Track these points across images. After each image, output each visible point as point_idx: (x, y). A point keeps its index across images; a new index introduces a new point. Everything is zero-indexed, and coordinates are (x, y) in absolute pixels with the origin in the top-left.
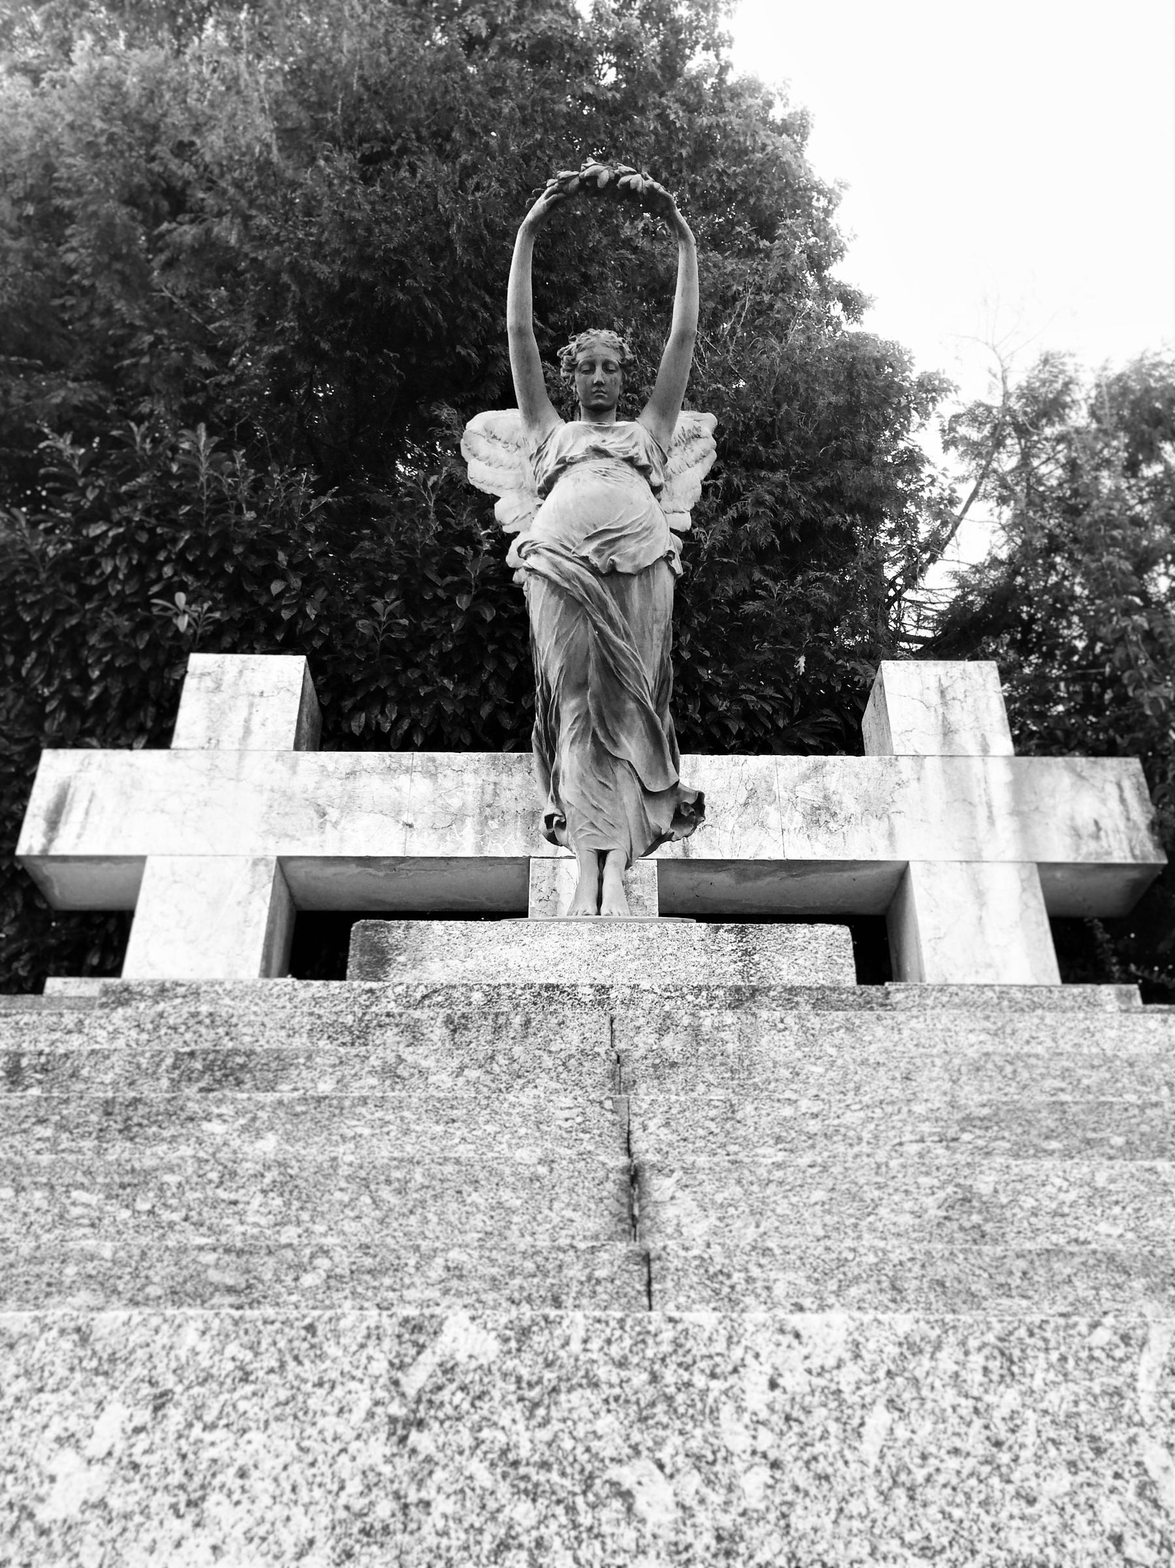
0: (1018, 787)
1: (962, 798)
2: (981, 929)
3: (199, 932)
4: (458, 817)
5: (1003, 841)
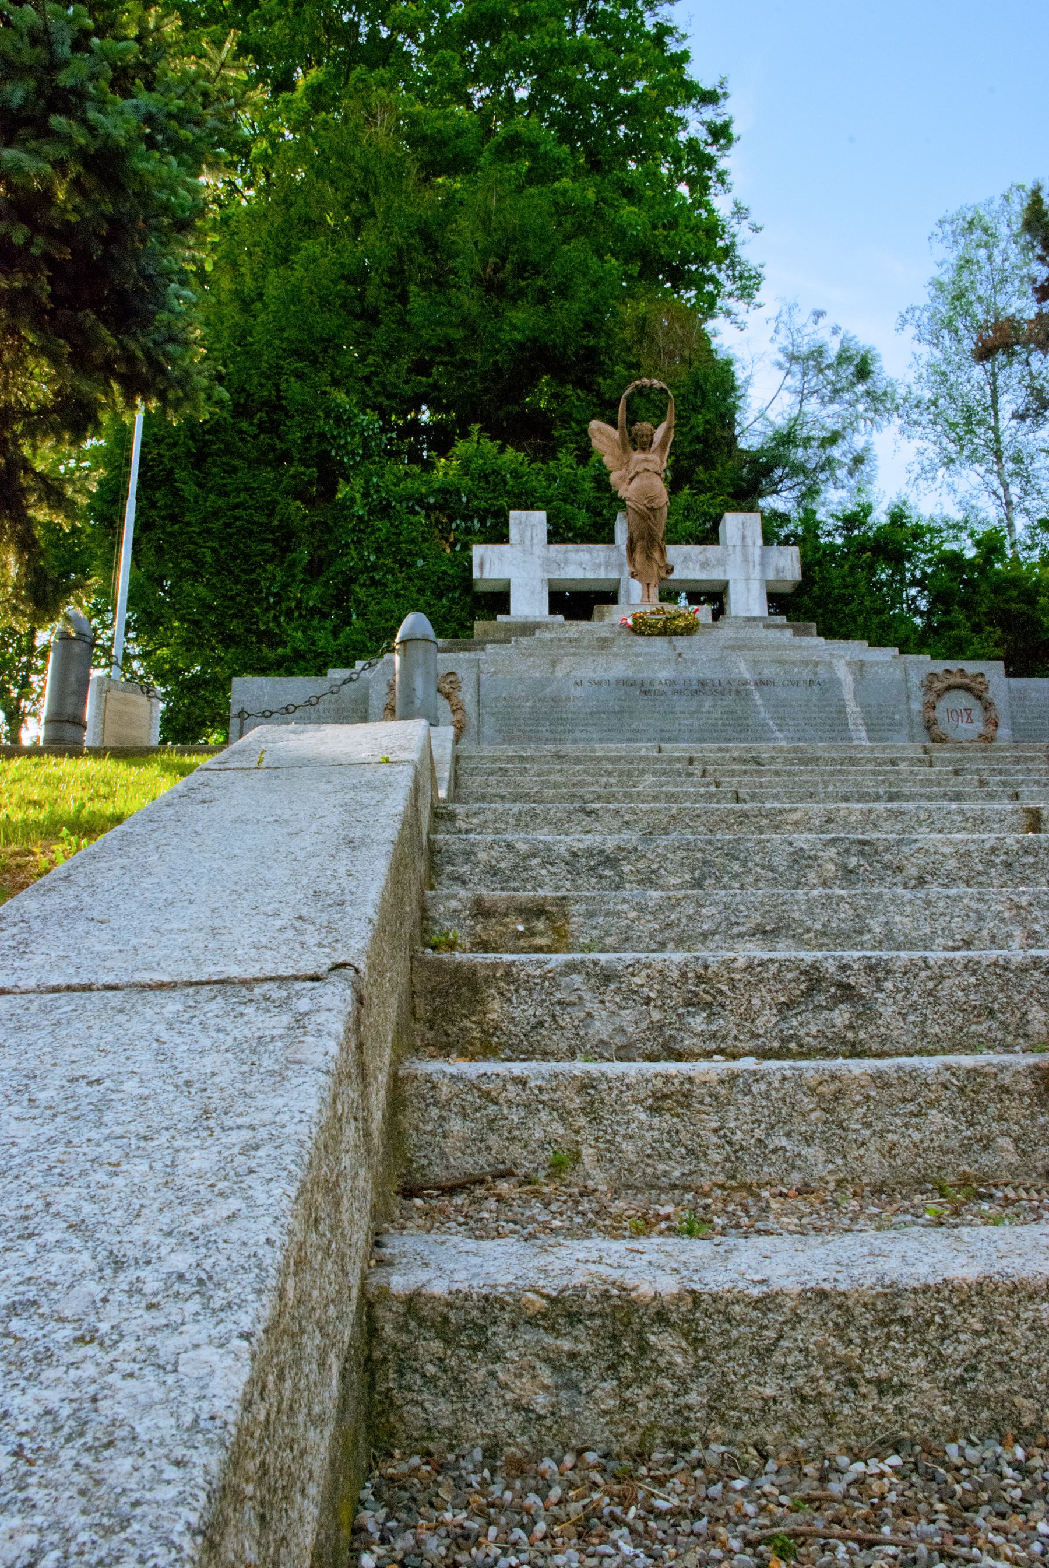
0: (763, 556)
1: (746, 559)
2: (747, 600)
3: (528, 604)
4: (599, 566)
5: (756, 573)
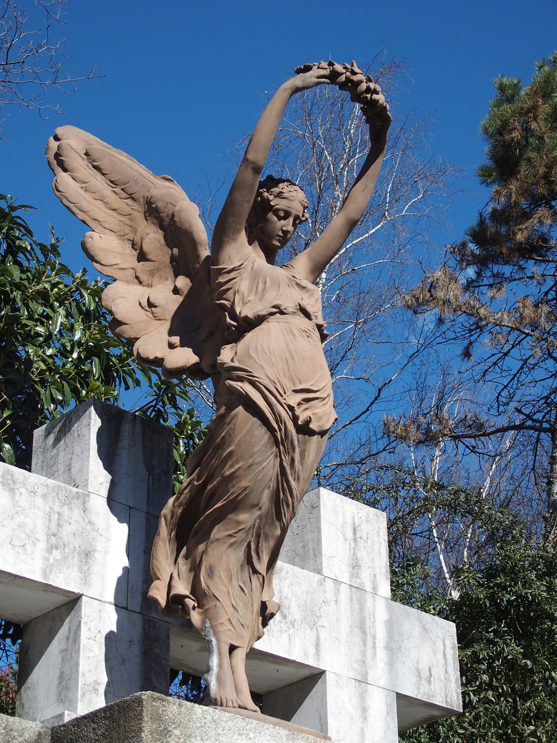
1: (362, 626)
5: (379, 673)
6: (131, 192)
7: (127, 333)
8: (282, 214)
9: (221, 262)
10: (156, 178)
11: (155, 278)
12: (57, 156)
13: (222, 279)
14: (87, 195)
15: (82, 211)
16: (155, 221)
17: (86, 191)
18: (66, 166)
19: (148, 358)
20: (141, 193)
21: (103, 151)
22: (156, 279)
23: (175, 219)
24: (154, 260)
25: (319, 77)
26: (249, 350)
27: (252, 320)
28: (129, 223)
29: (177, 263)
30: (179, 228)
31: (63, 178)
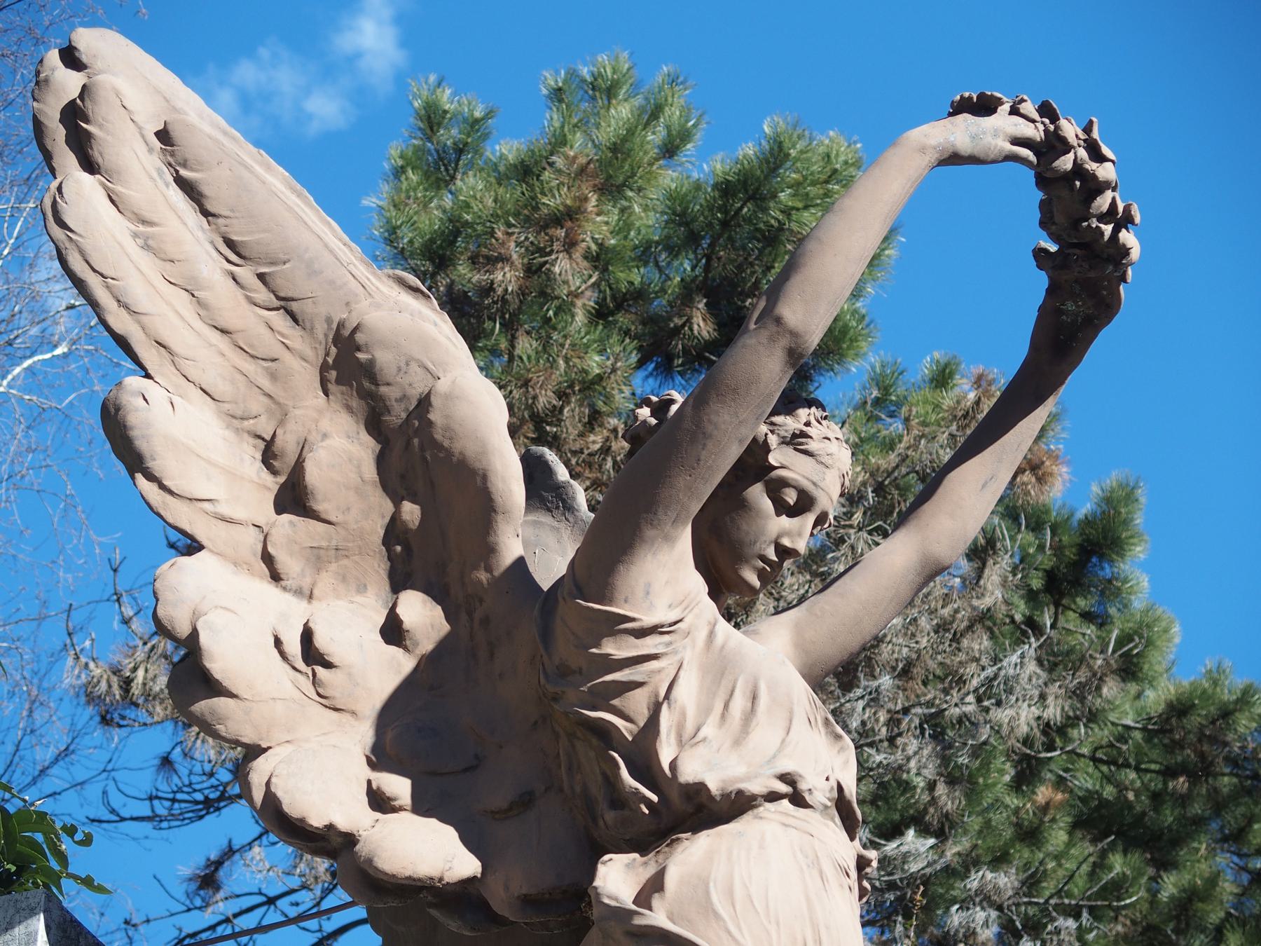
6: (290, 294)
7: (230, 724)
8: (791, 497)
9: (620, 596)
10: (374, 274)
11: (324, 574)
12: (74, 115)
13: (615, 648)
14: (145, 261)
15: (126, 307)
16: (355, 403)
17: (146, 247)
18: (96, 154)
19: (302, 820)
20: (324, 309)
21: (217, 141)
22: (325, 582)
23: (432, 416)
24: (332, 518)
25: (1017, 141)
26: (707, 893)
27: (711, 797)
28: (265, 383)
29: (407, 548)
30: (438, 446)
31: (82, 190)
